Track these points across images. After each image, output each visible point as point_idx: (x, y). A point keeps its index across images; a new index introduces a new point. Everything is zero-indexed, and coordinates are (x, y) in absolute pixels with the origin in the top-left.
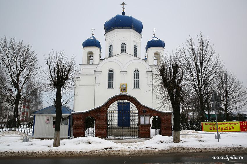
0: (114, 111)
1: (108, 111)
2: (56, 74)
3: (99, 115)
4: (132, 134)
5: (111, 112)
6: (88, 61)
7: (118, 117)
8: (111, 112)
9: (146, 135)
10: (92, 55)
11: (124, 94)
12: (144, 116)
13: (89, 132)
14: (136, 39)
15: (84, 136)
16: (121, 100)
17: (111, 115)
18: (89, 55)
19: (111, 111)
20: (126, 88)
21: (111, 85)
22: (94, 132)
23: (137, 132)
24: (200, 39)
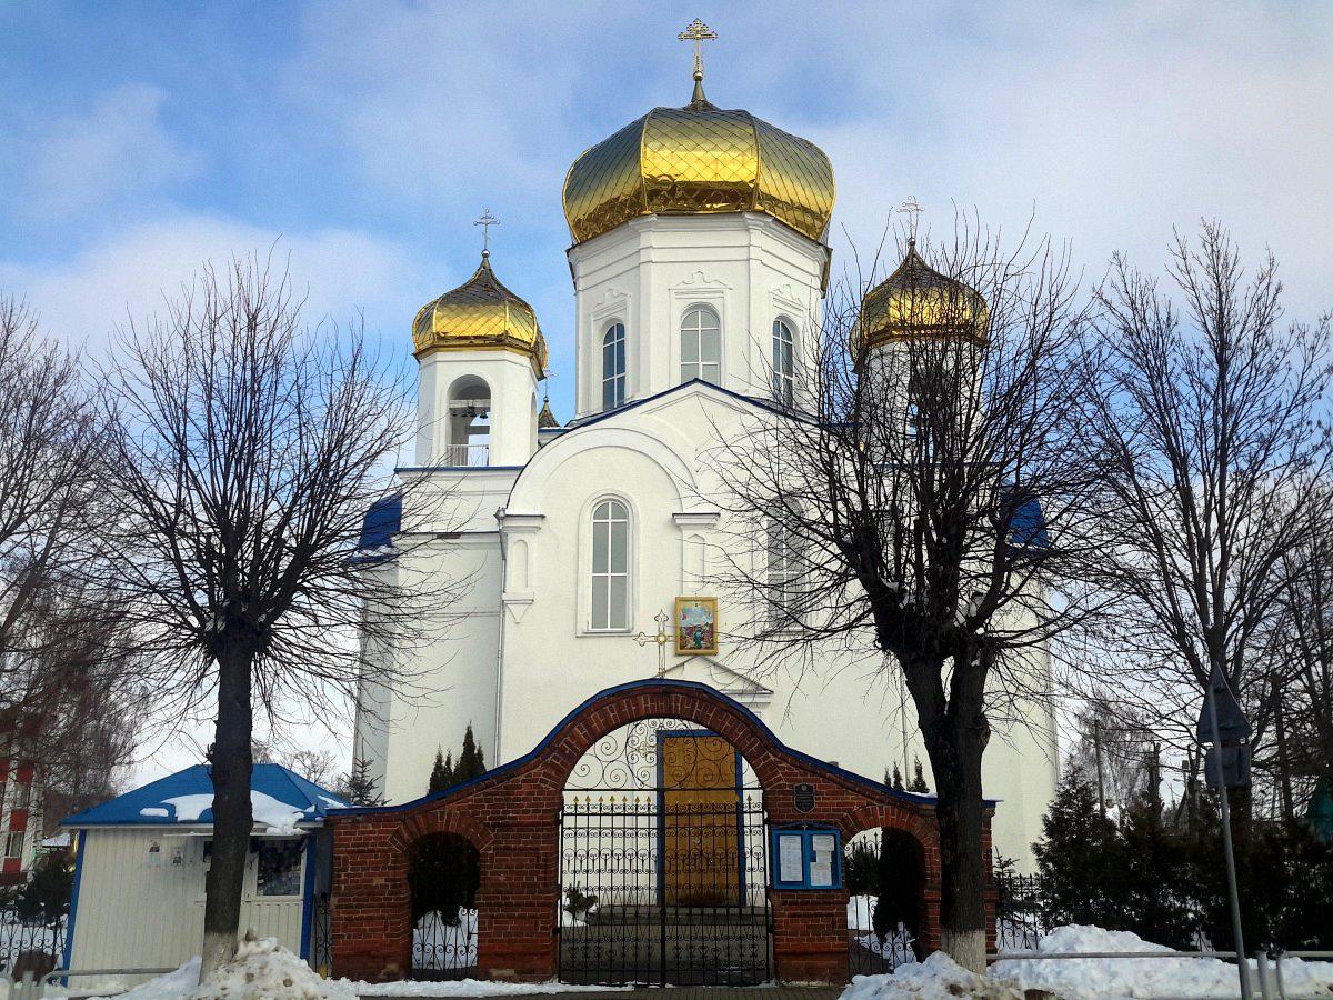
0: (607, 796)
1: (568, 798)
2: (248, 486)
3: (505, 827)
4: (722, 956)
5: (582, 801)
6: (454, 441)
7: (440, 833)
8: (582, 801)
9: (819, 963)
10: (478, 404)
11: (695, 672)
12: (799, 828)
13: (439, 942)
14: (786, 280)
15: (402, 967)
16: (648, 717)
17: (582, 821)
18: (462, 404)
19: (582, 796)
20: (712, 626)
21: (610, 611)
22: (474, 939)
23: (762, 944)
24: (1205, 281)
